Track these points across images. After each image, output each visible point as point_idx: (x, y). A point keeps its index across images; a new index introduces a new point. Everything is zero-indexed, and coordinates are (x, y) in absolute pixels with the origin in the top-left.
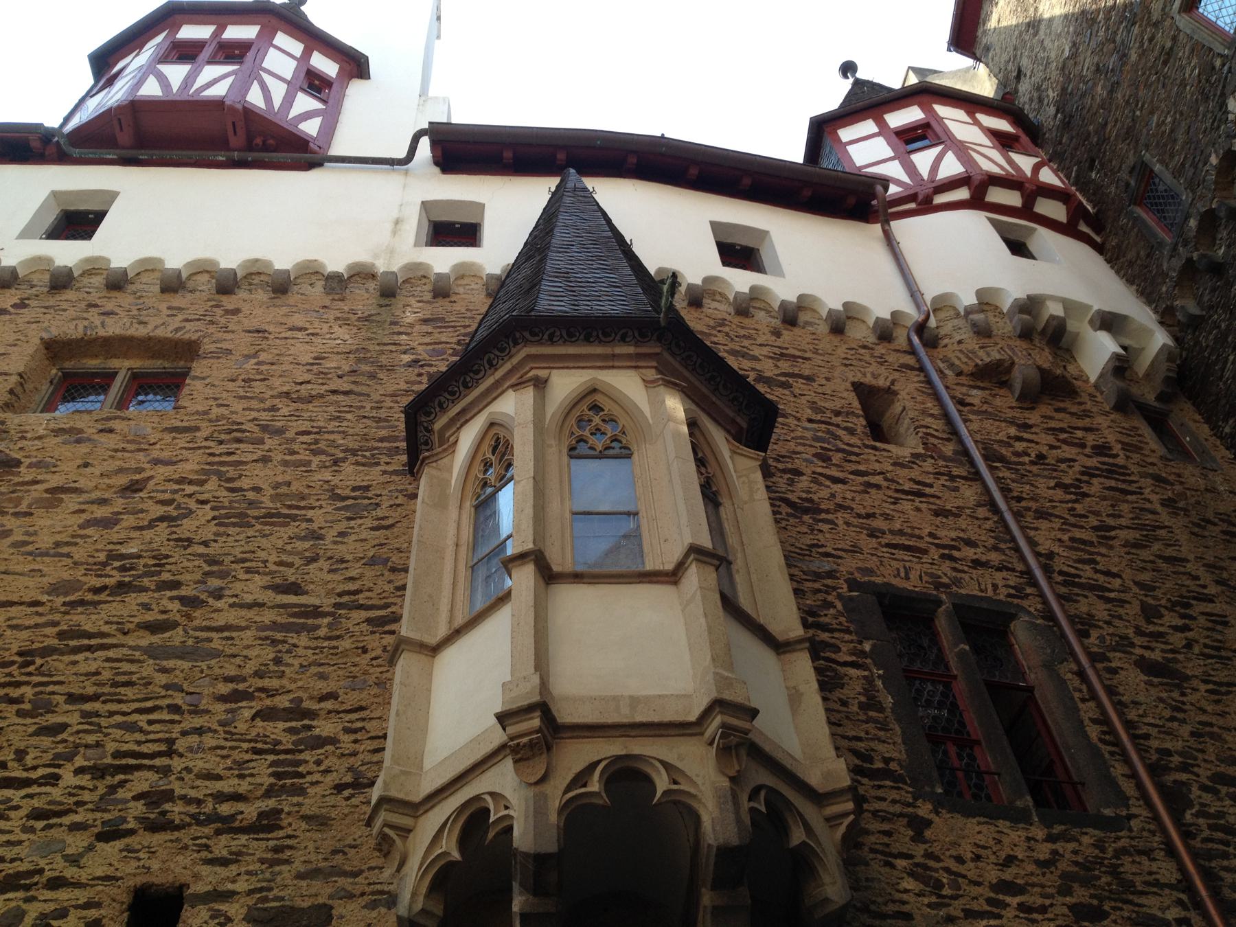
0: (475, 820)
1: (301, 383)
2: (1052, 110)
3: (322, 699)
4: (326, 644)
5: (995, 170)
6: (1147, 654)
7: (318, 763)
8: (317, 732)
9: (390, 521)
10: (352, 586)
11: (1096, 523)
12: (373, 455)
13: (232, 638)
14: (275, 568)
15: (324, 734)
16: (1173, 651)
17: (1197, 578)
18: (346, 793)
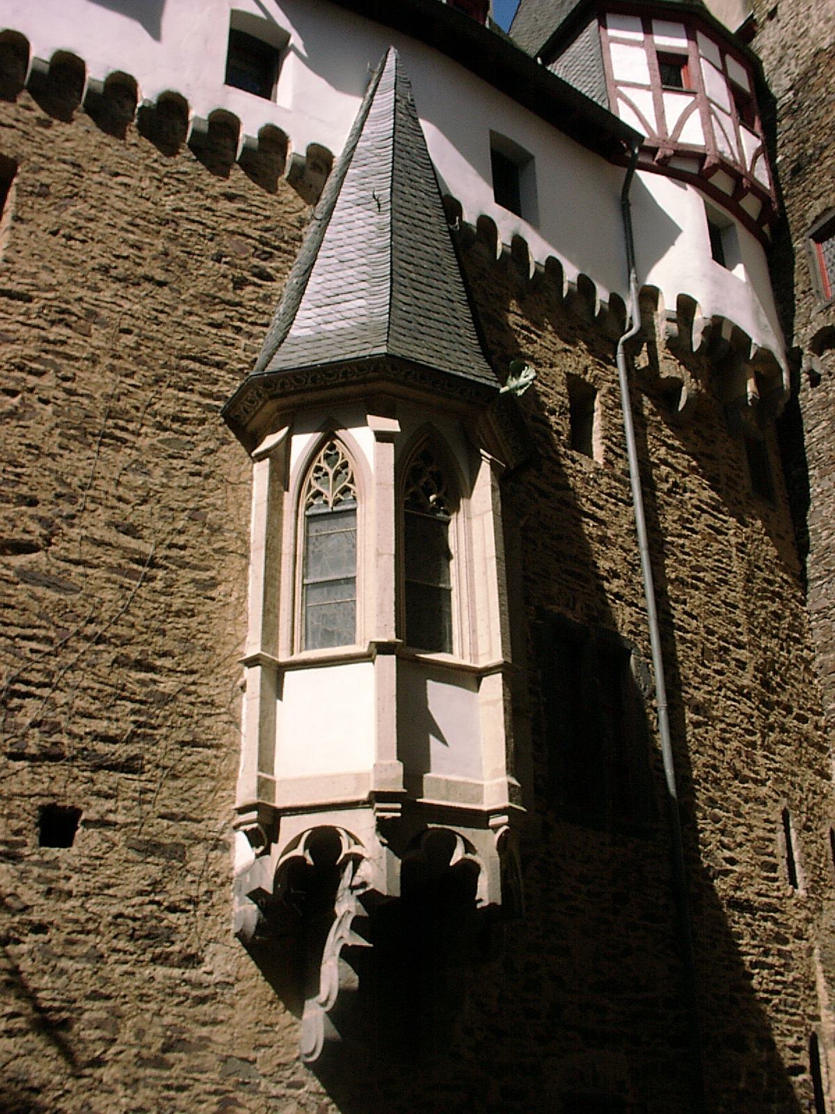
0: (325, 842)
1: (118, 257)
2: (786, 83)
3: (164, 654)
4: (162, 599)
5: (727, 154)
6: (696, 693)
7: (166, 718)
8: (161, 687)
9: (206, 470)
10: (181, 540)
11: (694, 563)
12: (189, 379)
13: (87, 576)
14: (115, 502)
15: (167, 691)
16: (710, 693)
17: (738, 625)
18: (187, 749)
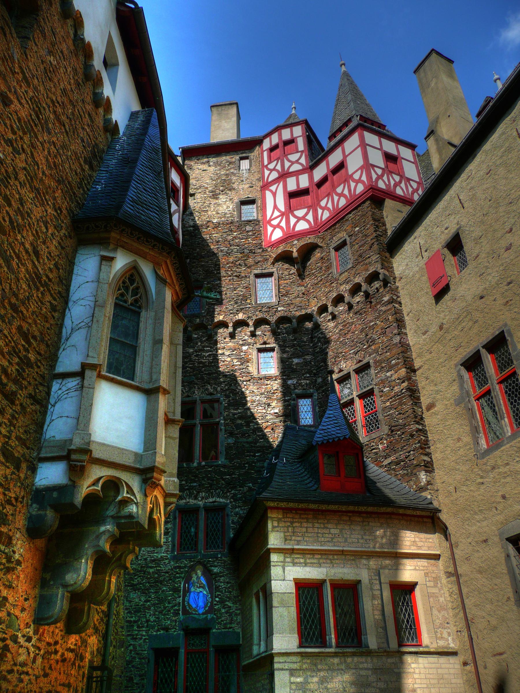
0: (113, 485)
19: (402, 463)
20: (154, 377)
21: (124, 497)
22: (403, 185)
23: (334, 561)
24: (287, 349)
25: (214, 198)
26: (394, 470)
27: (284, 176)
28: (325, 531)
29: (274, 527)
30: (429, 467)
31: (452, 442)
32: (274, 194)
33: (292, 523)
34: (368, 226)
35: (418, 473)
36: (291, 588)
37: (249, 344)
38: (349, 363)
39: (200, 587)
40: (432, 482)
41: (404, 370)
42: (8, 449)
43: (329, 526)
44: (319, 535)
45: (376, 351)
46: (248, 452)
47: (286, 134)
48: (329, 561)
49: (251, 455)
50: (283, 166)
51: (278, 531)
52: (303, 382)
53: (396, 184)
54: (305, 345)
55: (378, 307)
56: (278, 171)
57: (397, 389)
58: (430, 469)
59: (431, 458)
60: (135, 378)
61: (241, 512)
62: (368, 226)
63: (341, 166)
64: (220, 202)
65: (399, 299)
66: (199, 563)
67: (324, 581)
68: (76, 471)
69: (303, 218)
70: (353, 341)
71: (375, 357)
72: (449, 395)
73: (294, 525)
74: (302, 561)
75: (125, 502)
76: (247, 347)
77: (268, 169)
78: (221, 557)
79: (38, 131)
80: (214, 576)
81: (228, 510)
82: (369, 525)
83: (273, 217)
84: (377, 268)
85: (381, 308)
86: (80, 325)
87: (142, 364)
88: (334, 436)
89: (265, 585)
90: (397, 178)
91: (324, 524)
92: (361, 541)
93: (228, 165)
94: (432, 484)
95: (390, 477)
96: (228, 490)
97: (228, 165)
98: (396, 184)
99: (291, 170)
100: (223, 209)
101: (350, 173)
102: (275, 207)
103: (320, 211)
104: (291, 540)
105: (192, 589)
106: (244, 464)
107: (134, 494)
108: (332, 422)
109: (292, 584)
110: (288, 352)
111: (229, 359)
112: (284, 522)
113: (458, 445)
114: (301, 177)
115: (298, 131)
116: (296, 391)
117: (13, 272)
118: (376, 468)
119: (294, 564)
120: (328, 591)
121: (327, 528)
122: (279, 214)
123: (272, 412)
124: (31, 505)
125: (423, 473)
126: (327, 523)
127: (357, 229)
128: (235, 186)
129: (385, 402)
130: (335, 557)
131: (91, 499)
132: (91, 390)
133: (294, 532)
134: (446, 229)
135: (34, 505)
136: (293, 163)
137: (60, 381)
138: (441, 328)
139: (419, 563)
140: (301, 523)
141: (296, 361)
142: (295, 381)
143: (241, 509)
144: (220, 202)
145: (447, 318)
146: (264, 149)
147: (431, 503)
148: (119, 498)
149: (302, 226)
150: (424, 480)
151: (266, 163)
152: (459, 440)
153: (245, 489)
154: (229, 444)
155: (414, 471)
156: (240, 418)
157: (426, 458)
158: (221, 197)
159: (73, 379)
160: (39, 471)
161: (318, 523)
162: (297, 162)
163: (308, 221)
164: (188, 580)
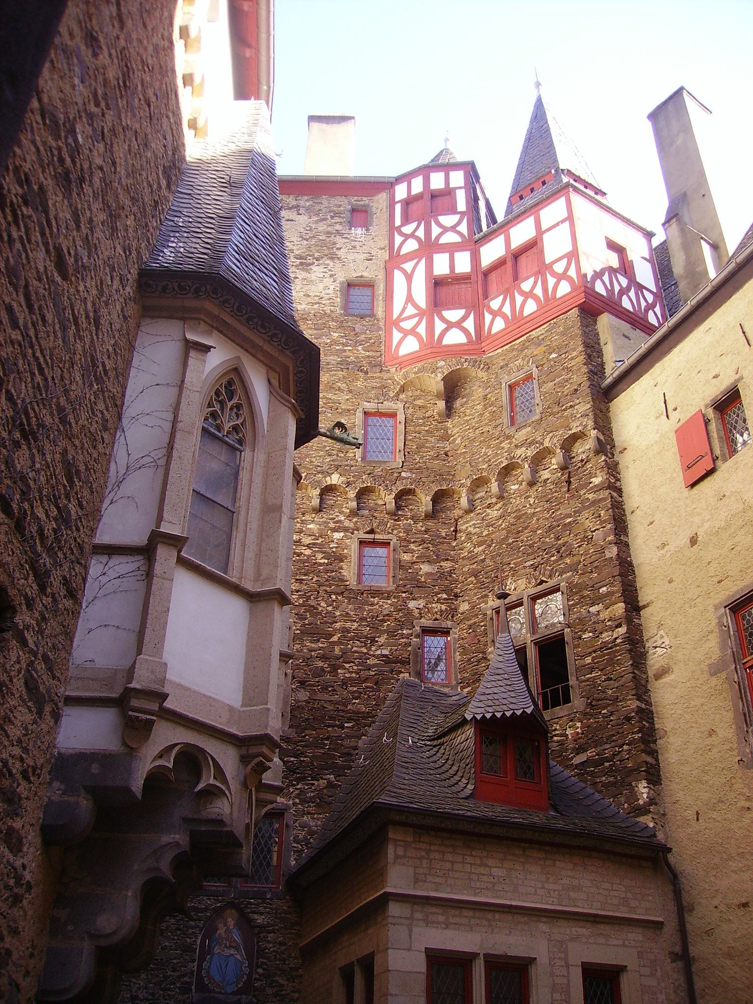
0: (191, 760)
19: (607, 764)
20: (265, 572)
21: (209, 785)
22: (632, 294)
23: (494, 923)
24: (412, 546)
25: (303, 270)
26: (592, 774)
27: (429, 248)
28: (482, 870)
29: (397, 857)
30: (654, 776)
31: (698, 735)
32: (409, 277)
33: (428, 852)
34: (575, 354)
35: (633, 784)
36: (419, 964)
37: (346, 530)
38: (522, 583)
39: (230, 947)
40: (657, 801)
41: (622, 605)
42: (32, 676)
43: (490, 862)
44: (473, 876)
45: (573, 568)
46: (331, 718)
47: (437, 181)
48: (485, 922)
49: (336, 726)
50: (428, 231)
51: (403, 864)
52: (437, 607)
53: (623, 291)
54: (442, 543)
55: (582, 492)
56: (418, 239)
57: (606, 637)
58: (655, 779)
59: (657, 760)
60: (230, 567)
61: (312, 823)
62: (575, 354)
63: (533, 246)
64: (313, 277)
65: (618, 484)
66: (232, 905)
67: (475, 955)
68: (136, 729)
69: (458, 325)
70: (531, 546)
71: (570, 577)
72: (699, 656)
73: (432, 857)
74: (441, 918)
75: (212, 793)
76: (342, 534)
77: (401, 234)
78: (271, 899)
79: (123, 107)
80: (256, 930)
81: (288, 818)
82: (554, 865)
83: (404, 315)
84: (586, 426)
85: (587, 496)
86: (143, 462)
87: (244, 544)
88: (505, 708)
89: (371, 956)
90: (624, 282)
91: (481, 858)
92: (541, 892)
93: (332, 217)
94: (656, 804)
95: (583, 785)
96: (291, 781)
97: (332, 217)
98: (623, 291)
99: (443, 240)
100: (317, 289)
101: (547, 261)
102: (410, 299)
103: (488, 318)
104: (425, 881)
105: (217, 950)
106: (322, 739)
107: (225, 781)
108: (500, 683)
109: (423, 957)
110: (412, 551)
111: (308, 552)
112: (415, 849)
113: (709, 741)
114: (457, 255)
115: (457, 178)
116: (423, 620)
117: (68, 351)
118: (559, 768)
119: (428, 923)
120: (479, 972)
121: (486, 865)
122: (415, 311)
123: (379, 652)
124: (50, 783)
125: (644, 783)
126: (487, 857)
127: (554, 355)
128: (340, 253)
129: (583, 657)
130: (497, 916)
131: (156, 780)
132: (167, 583)
133: (430, 868)
134: (716, 377)
135: (56, 784)
136: (445, 230)
137: (104, 559)
138: (693, 541)
139: (630, 936)
140: (444, 853)
141: (425, 568)
142: (421, 603)
143: (313, 818)
144: (313, 277)
145: (707, 525)
146: (397, 199)
147: (655, 836)
148: (201, 786)
149: (455, 337)
150: (645, 796)
151: (398, 222)
152: (712, 732)
153: (322, 783)
154: (297, 701)
155: (629, 779)
156: (323, 658)
157: (649, 759)
158: (314, 268)
159: (130, 559)
160: (64, 721)
161: (471, 855)
162: (453, 228)
163: (466, 331)
164: (210, 932)
